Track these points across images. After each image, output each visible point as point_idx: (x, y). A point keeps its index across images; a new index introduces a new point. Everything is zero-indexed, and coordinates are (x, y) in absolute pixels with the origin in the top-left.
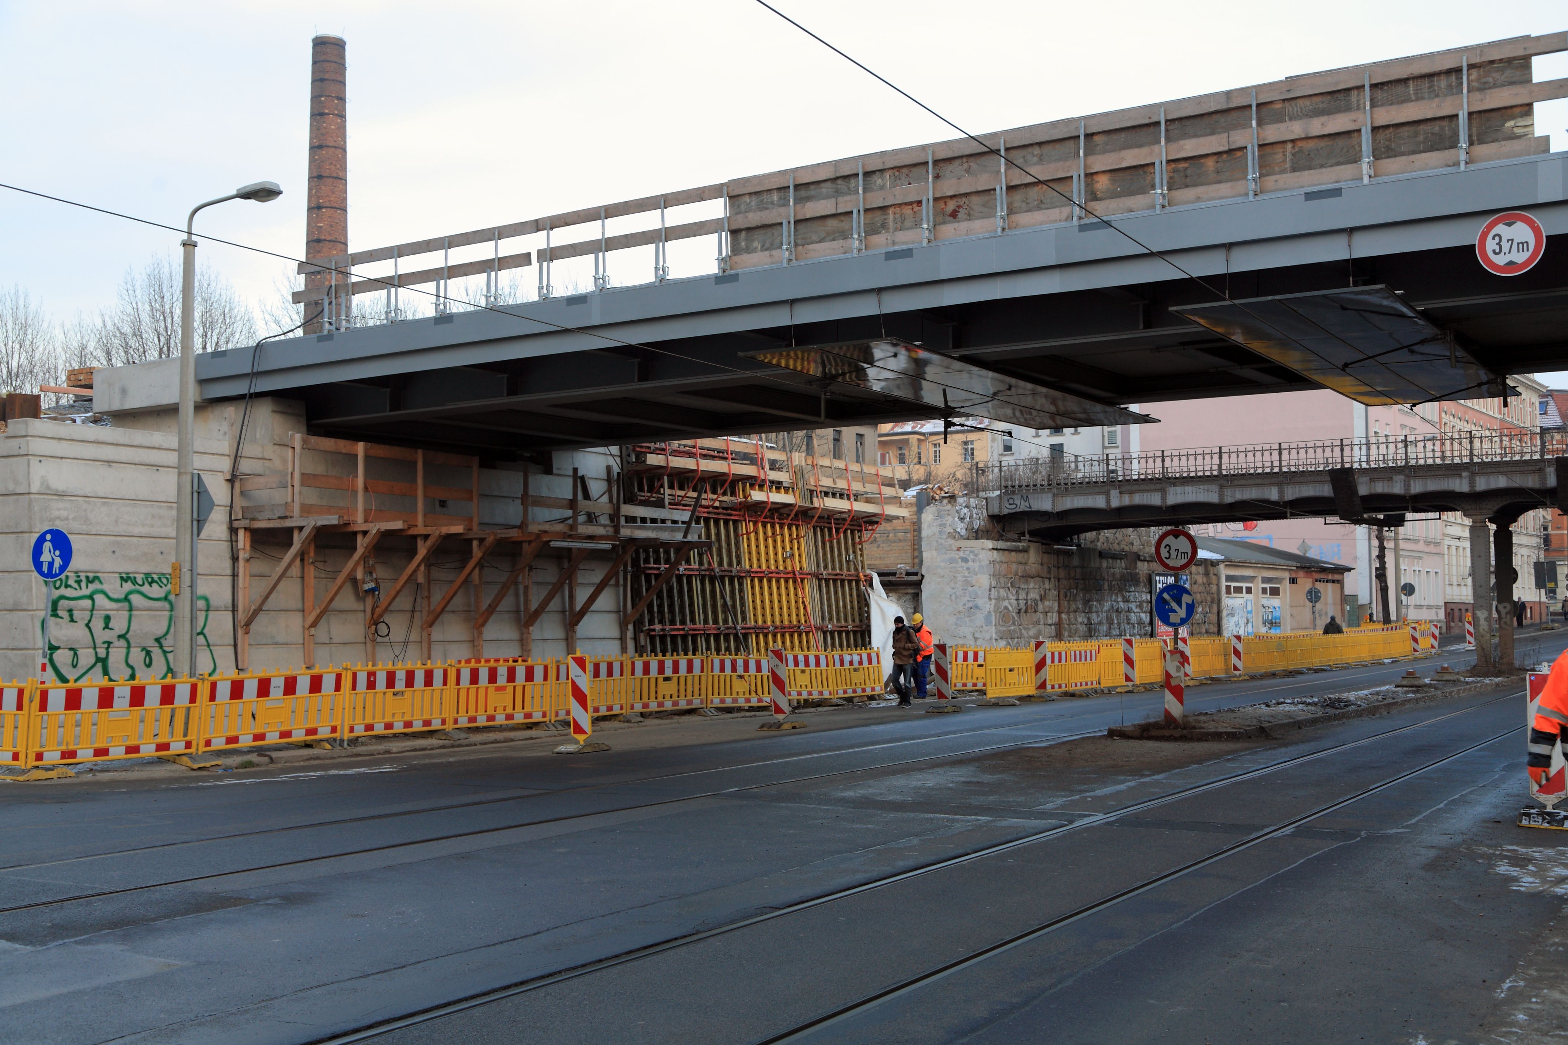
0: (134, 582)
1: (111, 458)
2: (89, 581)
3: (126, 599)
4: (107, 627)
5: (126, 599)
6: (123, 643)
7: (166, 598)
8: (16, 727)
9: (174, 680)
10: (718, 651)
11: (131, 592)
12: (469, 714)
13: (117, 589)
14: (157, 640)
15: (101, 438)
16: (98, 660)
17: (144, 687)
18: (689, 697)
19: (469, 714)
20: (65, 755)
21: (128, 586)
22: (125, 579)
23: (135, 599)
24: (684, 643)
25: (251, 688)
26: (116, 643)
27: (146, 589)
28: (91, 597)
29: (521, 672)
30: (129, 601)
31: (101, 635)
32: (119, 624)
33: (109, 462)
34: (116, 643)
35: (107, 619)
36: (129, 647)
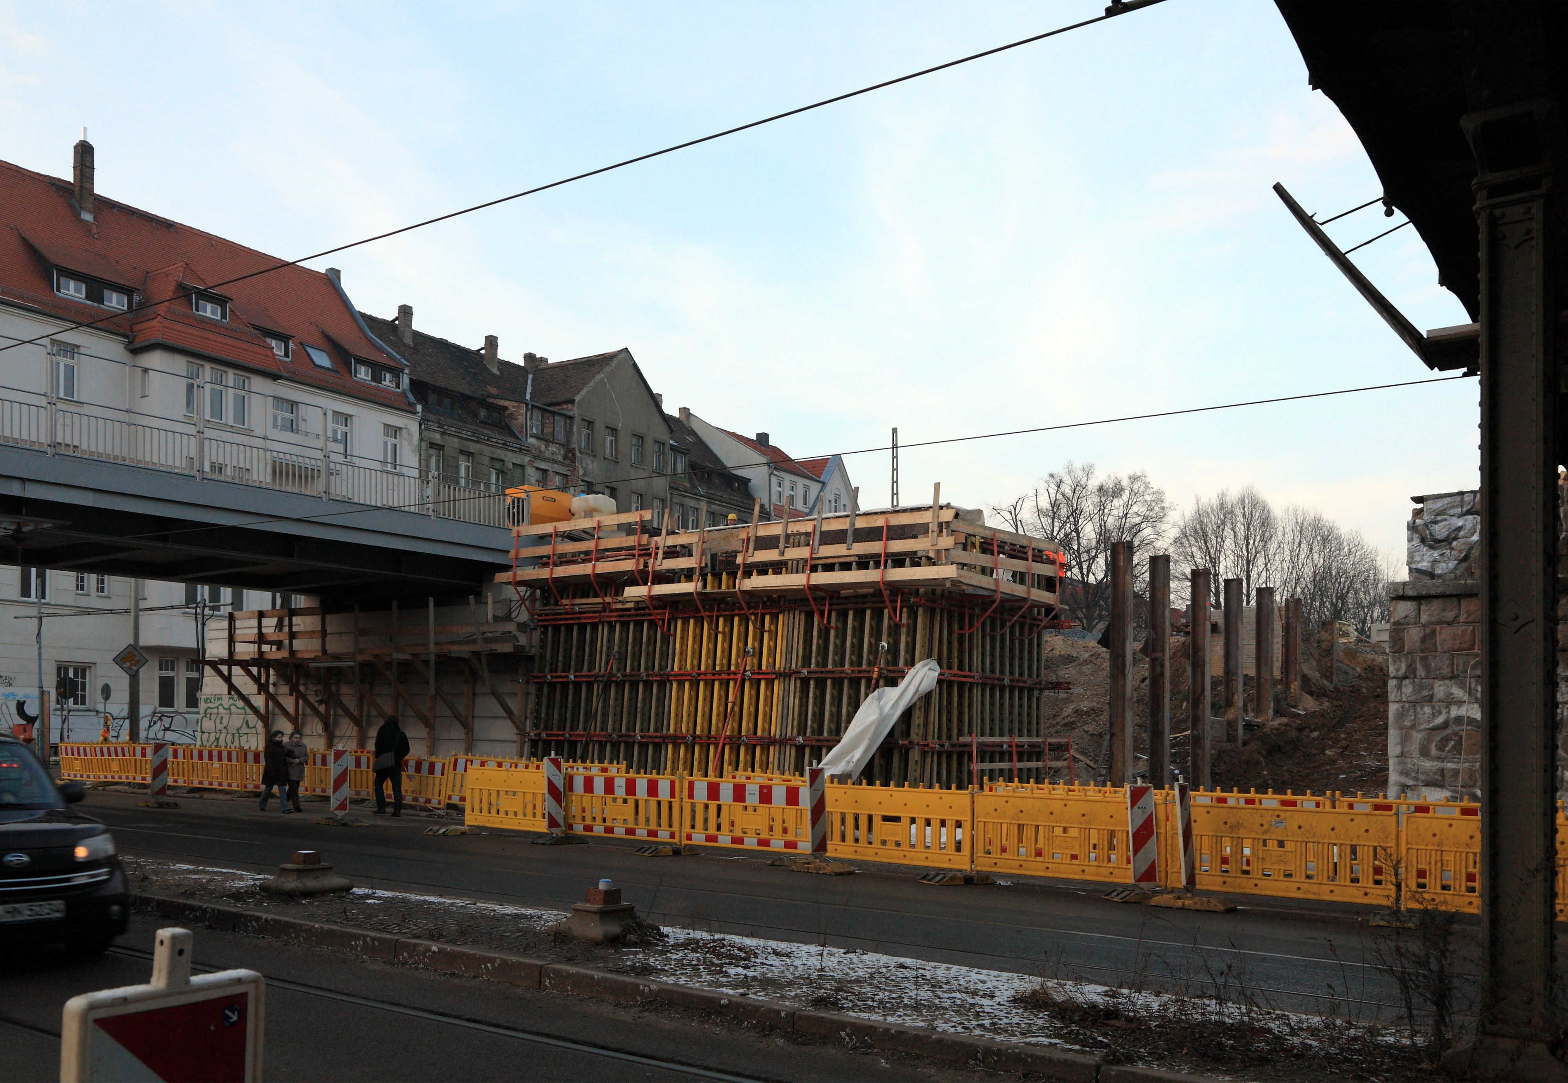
32: (225, 721)
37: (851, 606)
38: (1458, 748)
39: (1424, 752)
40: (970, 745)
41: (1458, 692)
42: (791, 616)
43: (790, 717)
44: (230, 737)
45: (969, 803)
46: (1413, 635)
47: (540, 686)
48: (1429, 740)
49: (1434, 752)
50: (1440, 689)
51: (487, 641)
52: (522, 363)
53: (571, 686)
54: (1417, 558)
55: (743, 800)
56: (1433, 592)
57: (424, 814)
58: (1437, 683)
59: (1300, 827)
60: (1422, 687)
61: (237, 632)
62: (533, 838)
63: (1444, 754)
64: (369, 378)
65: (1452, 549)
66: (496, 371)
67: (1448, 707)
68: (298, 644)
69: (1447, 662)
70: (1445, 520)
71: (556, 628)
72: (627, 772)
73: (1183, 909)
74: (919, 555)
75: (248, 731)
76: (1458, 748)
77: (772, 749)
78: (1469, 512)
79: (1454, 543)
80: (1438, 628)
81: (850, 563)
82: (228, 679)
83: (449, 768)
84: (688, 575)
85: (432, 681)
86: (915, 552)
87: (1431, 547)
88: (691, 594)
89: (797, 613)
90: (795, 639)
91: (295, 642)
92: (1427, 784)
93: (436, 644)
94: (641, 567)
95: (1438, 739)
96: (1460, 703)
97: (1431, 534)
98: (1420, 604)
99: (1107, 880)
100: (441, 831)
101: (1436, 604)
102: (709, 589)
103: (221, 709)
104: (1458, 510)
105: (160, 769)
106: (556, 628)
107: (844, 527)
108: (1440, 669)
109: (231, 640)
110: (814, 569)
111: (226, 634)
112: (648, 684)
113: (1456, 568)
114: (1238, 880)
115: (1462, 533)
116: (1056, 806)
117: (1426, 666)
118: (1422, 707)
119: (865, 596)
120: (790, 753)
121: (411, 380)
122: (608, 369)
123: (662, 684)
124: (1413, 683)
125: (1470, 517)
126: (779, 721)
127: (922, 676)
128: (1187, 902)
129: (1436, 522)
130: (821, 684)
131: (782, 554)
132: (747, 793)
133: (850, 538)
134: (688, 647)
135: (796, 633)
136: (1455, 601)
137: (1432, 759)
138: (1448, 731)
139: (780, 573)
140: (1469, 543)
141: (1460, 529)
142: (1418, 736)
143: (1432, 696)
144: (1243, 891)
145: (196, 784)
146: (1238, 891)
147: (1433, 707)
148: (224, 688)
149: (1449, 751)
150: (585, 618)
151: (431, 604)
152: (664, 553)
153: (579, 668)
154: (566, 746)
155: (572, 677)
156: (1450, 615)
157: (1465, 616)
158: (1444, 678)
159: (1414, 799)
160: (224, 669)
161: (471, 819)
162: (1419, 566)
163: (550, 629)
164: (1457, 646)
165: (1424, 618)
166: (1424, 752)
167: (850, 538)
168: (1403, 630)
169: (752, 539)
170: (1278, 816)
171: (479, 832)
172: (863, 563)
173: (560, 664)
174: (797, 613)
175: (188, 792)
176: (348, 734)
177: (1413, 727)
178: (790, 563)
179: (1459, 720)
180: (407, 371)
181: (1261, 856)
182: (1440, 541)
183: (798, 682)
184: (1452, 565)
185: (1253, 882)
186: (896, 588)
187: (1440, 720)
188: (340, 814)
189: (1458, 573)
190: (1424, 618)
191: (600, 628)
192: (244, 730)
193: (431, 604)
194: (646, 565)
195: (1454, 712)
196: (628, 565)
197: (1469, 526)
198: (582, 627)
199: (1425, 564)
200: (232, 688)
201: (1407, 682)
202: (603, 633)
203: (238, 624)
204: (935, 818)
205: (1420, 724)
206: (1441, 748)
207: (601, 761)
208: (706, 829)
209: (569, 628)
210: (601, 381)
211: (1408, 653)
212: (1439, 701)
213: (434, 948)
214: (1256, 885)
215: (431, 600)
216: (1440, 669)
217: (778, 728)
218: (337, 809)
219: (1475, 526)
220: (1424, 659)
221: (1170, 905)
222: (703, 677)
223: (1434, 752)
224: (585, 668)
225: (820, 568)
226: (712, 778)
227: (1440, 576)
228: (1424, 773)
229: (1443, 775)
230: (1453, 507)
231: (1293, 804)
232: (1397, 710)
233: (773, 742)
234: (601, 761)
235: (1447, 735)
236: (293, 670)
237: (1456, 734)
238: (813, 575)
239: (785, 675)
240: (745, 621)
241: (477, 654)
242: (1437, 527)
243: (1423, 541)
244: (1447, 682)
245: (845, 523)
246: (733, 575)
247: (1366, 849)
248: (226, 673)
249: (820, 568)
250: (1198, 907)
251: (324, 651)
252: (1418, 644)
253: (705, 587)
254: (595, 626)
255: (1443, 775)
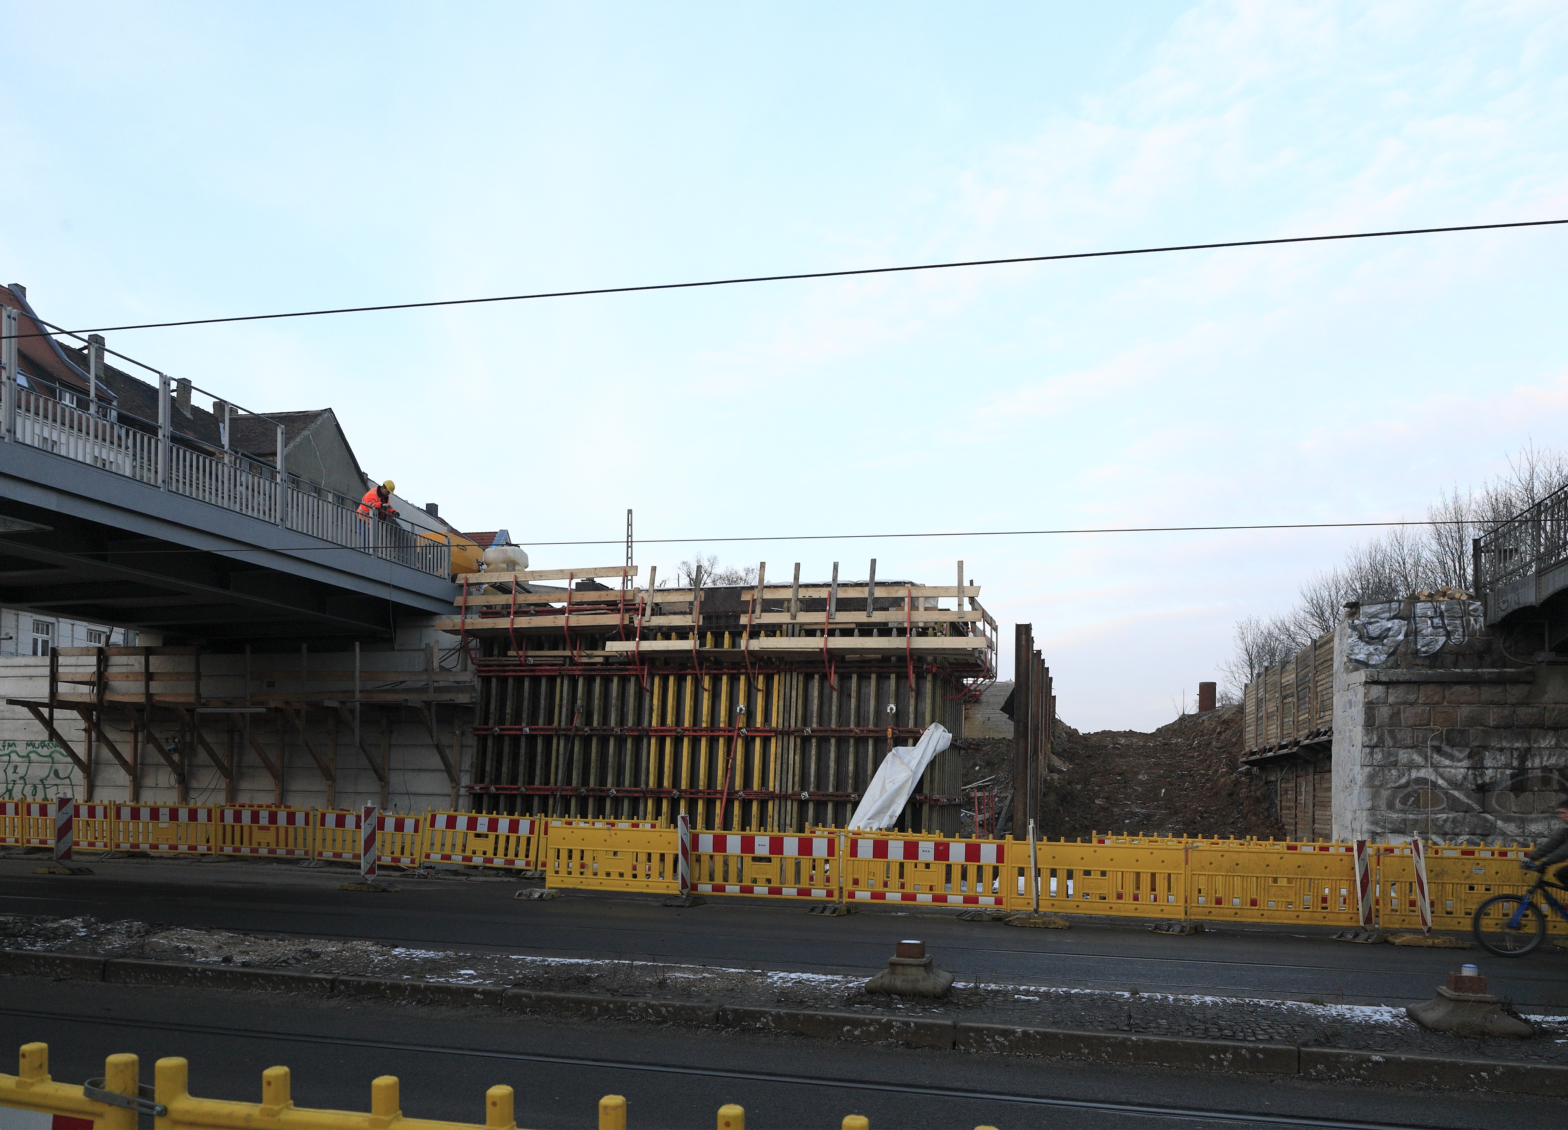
0: (34, 746)
1: (32, 674)
2: (10, 746)
3: (28, 756)
4: (15, 772)
5: (28, 756)
6: (22, 781)
7: (50, 756)
8: (334, 840)
9: (782, 834)
10: (745, 823)
11: (31, 752)
12: (508, 857)
13: (22, 749)
14: (41, 780)
15: (28, 664)
16: (8, 790)
17: (754, 838)
18: (237, 844)
19: (508, 857)
20: (190, 848)
21: (30, 748)
22: (30, 744)
23: (33, 756)
24: (525, 804)
25: (145, 813)
26: (19, 782)
27: (40, 750)
28: (9, 755)
29: (282, 817)
30: (53, 758)
31: (11, 777)
32: (21, 771)
33: (31, 677)
34: (19, 782)
35: (16, 767)
36: (26, 784)
37: (689, 671)
38: (1417, 803)
39: (1391, 806)
40: (973, 798)
41: (1418, 759)
42: (788, 677)
43: (791, 773)
44: (29, 789)
45: (1183, 857)
46: (1384, 712)
47: (483, 740)
48: (1394, 797)
49: (1398, 805)
50: (1403, 756)
51: (438, 690)
52: (211, 411)
53: (523, 740)
54: (1356, 651)
55: (885, 856)
56: (1401, 679)
57: (398, 874)
58: (1401, 752)
59: (1497, 873)
60: (1390, 754)
61: (60, 670)
62: (665, 901)
63: (1407, 808)
64: (74, 406)
65: (1383, 645)
66: (189, 416)
67: (1409, 770)
68: (155, 687)
69: (1411, 734)
70: (1378, 622)
71: (503, 681)
72: (743, 829)
73: (1432, 947)
74: (890, 626)
75: (58, 782)
76: (1417, 803)
77: (770, 804)
78: (1395, 617)
79: (1385, 641)
80: (1402, 707)
81: (853, 630)
82: (48, 723)
83: (425, 826)
84: (682, 633)
85: (357, 731)
86: (886, 624)
87: (1368, 643)
88: (691, 651)
89: (795, 675)
90: (794, 700)
91: (152, 684)
92: (1393, 832)
93: (361, 692)
94: (627, 622)
95: (1401, 795)
96: (1419, 767)
97: (1367, 632)
98: (1388, 688)
99: (1258, 920)
100: (536, 896)
101: (1401, 689)
102: (709, 646)
103: (14, 757)
104: (1387, 615)
105: (64, 829)
106: (503, 681)
107: (862, 596)
108: (1404, 740)
109: (54, 679)
110: (832, 633)
111: (47, 671)
112: (621, 741)
113: (1386, 660)
114: (1443, 919)
115: (1391, 633)
116: (1273, 859)
117: (1394, 738)
118: (1390, 770)
119: (869, 661)
120: (791, 808)
121: (119, 414)
122: (313, 426)
123: (638, 741)
124: (1383, 751)
125: (1396, 621)
126: (778, 777)
127: (935, 738)
128: (1436, 941)
129: (1371, 623)
130: (823, 741)
131: (794, 617)
132: (920, 850)
133: (870, 607)
134: (663, 703)
135: (794, 693)
136: (1416, 687)
137: (1396, 812)
138: (1409, 789)
139: (774, 636)
140: (1396, 641)
141: (1389, 629)
142: (1385, 794)
143: (1396, 761)
144: (1448, 928)
145: (35, 843)
146: (1443, 928)
147: (1399, 771)
148: (45, 735)
149: (1411, 805)
150: (540, 671)
151: (358, 650)
152: (653, 610)
153: (533, 720)
154: (519, 801)
155: (527, 730)
156: (1412, 697)
157: (1424, 698)
158: (1407, 748)
159: (1381, 844)
160: (45, 711)
161: (553, 882)
162: (1358, 657)
163: (494, 681)
164: (1418, 723)
165: (1391, 699)
166: (1391, 806)
167: (870, 607)
168: (1373, 709)
169: (759, 601)
170: (1478, 864)
171: (569, 895)
172: (865, 630)
173: (508, 717)
174: (795, 675)
175: (25, 853)
176: (212, 786)
177: (1381, 786)
178: (784, 627)
179: (1418, 780)
180: (115, 403)
181: (1463, 898)
182: (1373, 638)
183: (799, 741)
184: (1383, 657)
185: (1456, 921)
186: (919, 656)
187: (1403, 781)
188: (370, 878)
189: (1389, 664)
190: (1391, 699)
191: (559, 681)
192: (52, 780)
193: (358, 650)
194: (631, 621)
195: (1414, 774)
196: (612, 619)
197: (1396, 628)
198: (536, 681)
199: (1362, 656)
200: (54, 734)
201: (1377, 750)
202: (563, 688)
203: (61, 660)
204: (1096, 868)
205: (1387, 783)
206: (1404, 801)
207: (511, 813)
208: (741, 881)
209: (519, 681)
210: (307, 438)
211: (1379, 727)
212: (1403, 765)
213: (1376, 1058)
214: (1459, 923)
215: (357, 643)
216: (1404, 740)
217: (777, 784)
218: (367, 873)
219: (1400, 628)
220: (1391, 732)
221: (1421, 944)
222: (595, 732)
223: (1398, 805)
224: (541, 721)
225: (837, 632)
226: (718, 831)
227: (1373, 666)
228: (1390, 823)
229: (1405, 825)
230: (1383, 612)
231: (1295, 848)
232: (1370, 772)
233: (773, 796)
234: (511, 813)
235: (1409, 793)
236: (145, 717)
237: (1415, 791)
238: (830, 639)
239: (784, 733)
240: (733, 681)
241: (428, 704)
242: (1370, 627)
243: (1360, 638)
244: (1409, 750)
245: (863, 592)
246: (736, 635)
247: (1463, 886)
248: (47, 715)
249: (837, 632)
250: (1448, 945)
251: (198, 695)
252: (1386, 720)
253: (703, 644)
254: (552, 680)
255: (1405, 825)
